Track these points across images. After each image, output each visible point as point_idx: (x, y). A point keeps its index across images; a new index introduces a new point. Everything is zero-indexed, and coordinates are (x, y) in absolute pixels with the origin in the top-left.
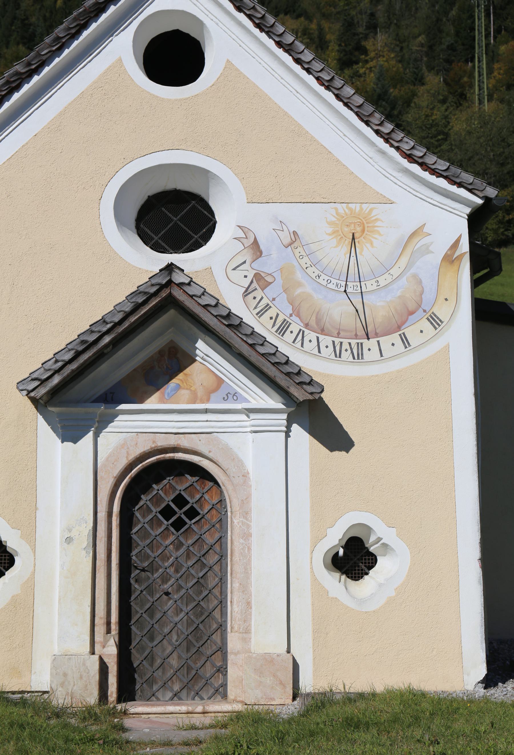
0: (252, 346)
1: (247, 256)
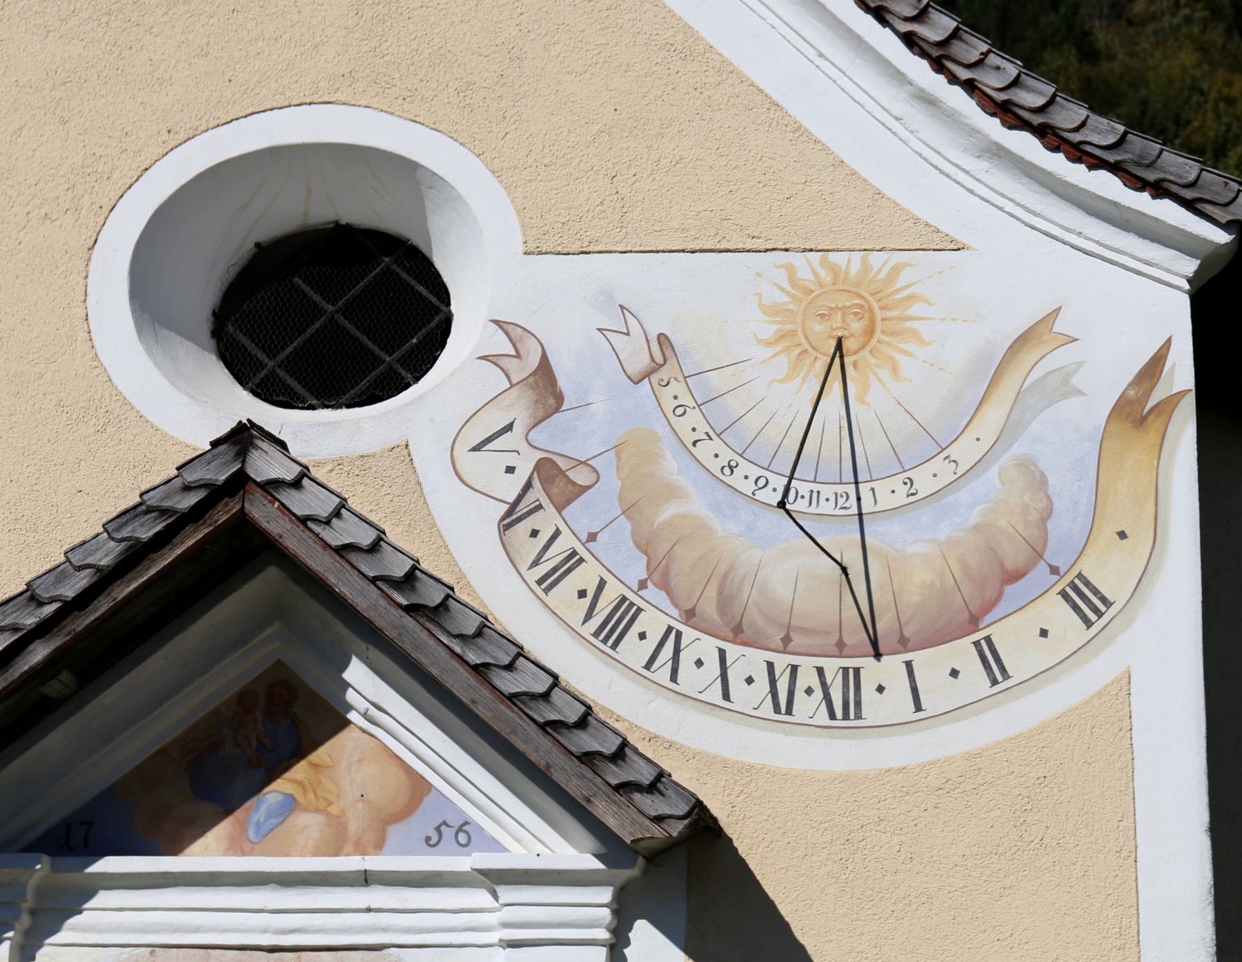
0: (480, 670)
1: (518, 410)
